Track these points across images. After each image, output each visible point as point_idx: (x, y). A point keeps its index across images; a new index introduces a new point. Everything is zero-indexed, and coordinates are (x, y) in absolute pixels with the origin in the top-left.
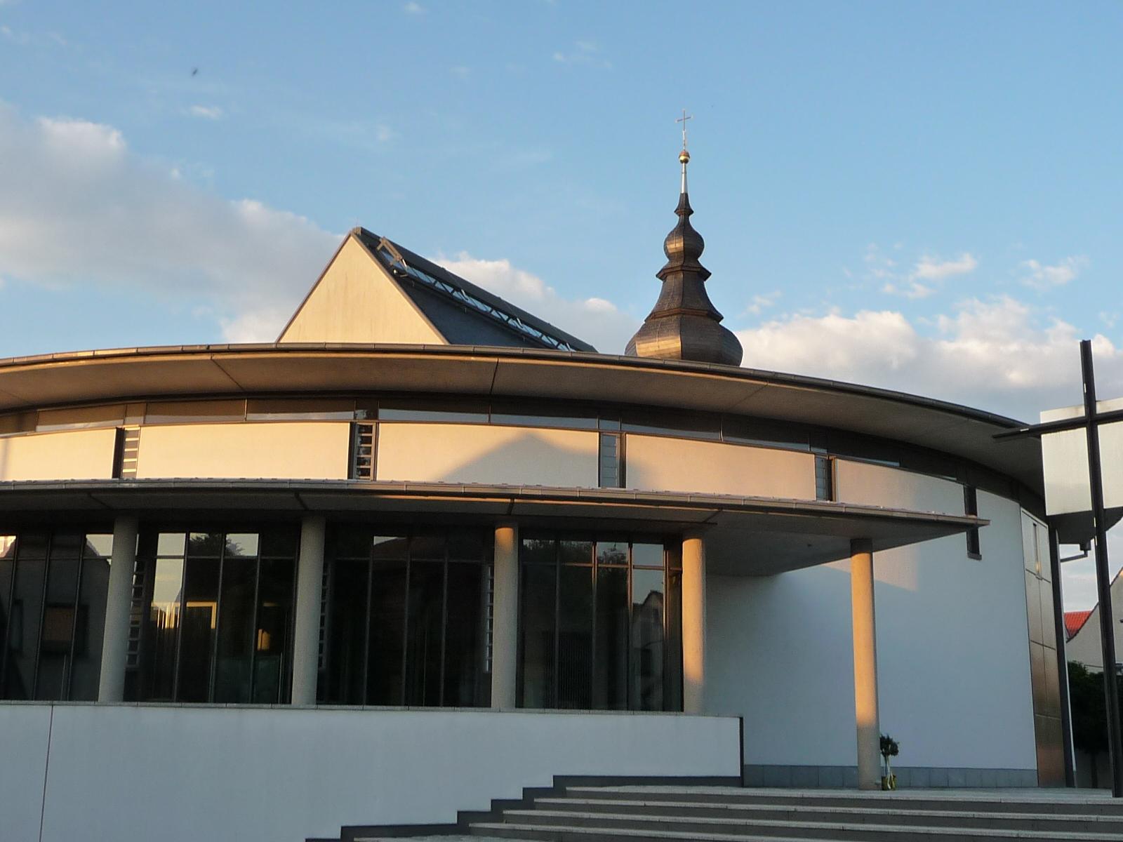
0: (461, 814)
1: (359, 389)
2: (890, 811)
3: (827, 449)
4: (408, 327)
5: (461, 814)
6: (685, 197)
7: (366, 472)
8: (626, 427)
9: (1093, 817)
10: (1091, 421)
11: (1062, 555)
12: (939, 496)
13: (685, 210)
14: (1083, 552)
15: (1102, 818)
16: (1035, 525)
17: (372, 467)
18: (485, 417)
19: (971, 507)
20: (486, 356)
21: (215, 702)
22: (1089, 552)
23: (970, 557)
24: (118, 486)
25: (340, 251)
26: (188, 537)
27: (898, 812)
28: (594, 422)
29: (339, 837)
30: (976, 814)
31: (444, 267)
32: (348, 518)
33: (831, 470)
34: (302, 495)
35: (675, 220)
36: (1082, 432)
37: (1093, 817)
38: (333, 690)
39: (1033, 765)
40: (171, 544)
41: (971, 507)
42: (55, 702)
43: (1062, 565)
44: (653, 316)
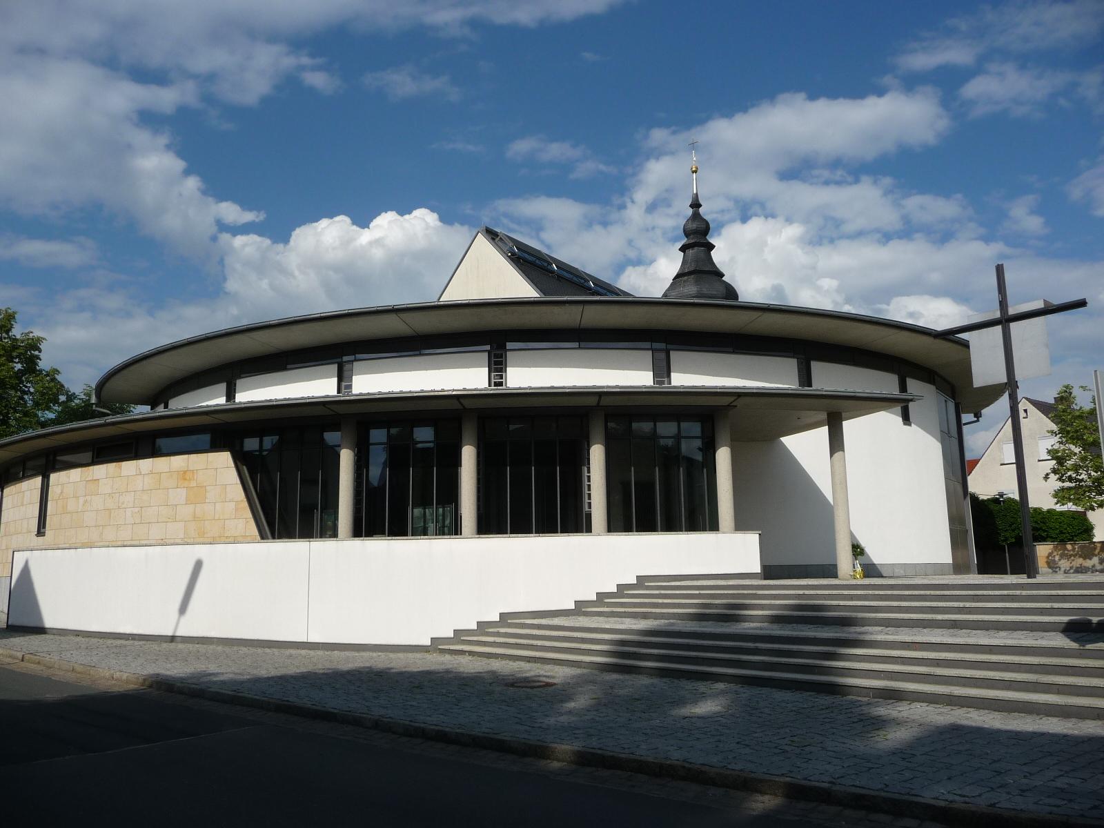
0: (501, 615)
1: (488, 332)
2: (870, 592)
3: (581, 466)
4: (518, 287)
5: (501, 615)
6: (696, 197)
7: (501, 384)
8: (669, 347)
9: (1018, 592)
10: (1005, 321)
11: (964, 421)
12: (885, 383)
13: (696, 205)
14: (976, 419)
15: (1024, 593)
16: (946, 401)
17: (503, 380)
18: (576, 345)
19: (903, 388)
20: (570, 308)
21: (412, 535)
22: (980, 418)
23: (905, 424)
24: (342, 399)
25: (472, 243)
26: (388, 431)
27: (877, 592)
28: (648, 345)
29: (498, 620)
30: (933, 593)
31: (151, 669)
32: (492, 417)
33: (757, 393)
34: (462, 401)
35: (690, 212)
36: (999, 328)
37: (1018, 592)
38: (489, 524)
39: (950, 561)
40: (378, 435)
41: (903, 388)
42: (311, 540)
43: (965, 428)
44: (678, 276)
